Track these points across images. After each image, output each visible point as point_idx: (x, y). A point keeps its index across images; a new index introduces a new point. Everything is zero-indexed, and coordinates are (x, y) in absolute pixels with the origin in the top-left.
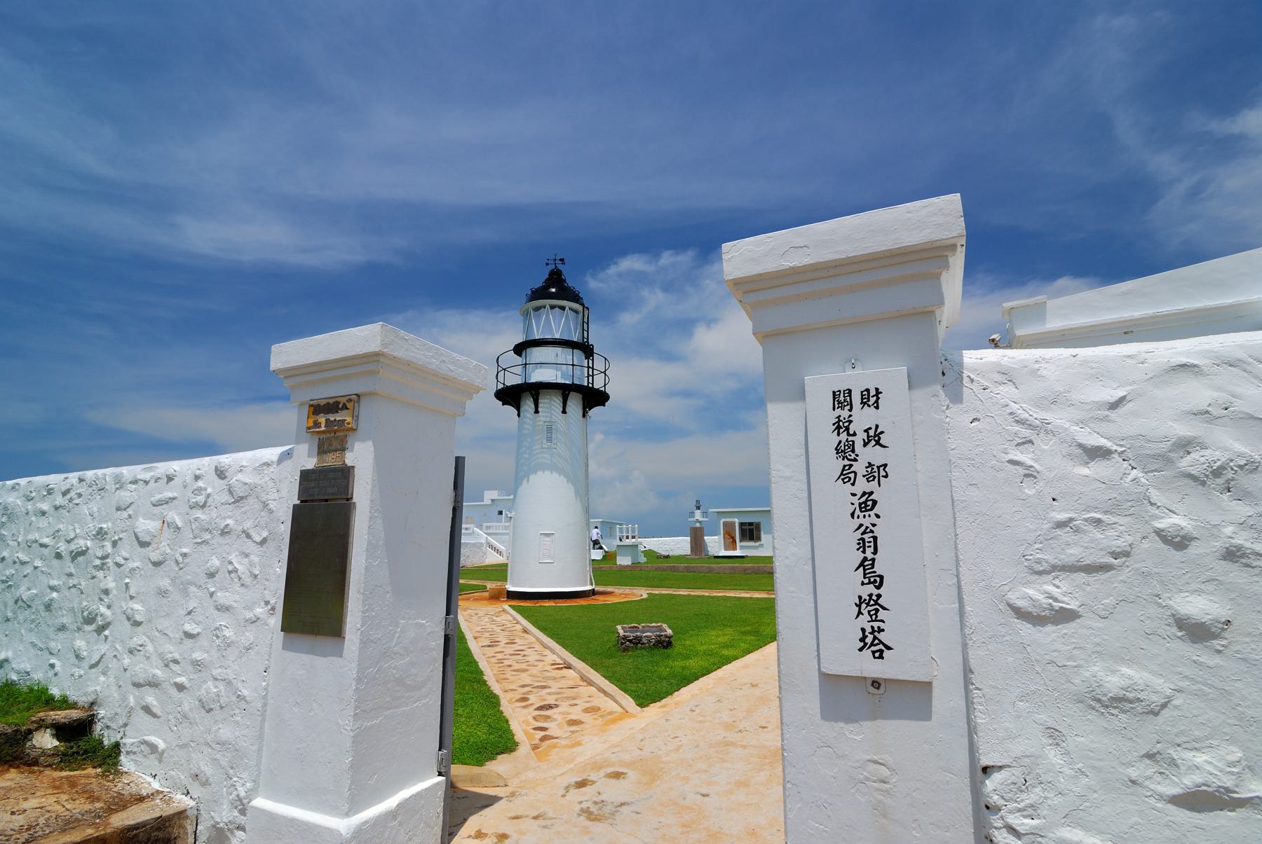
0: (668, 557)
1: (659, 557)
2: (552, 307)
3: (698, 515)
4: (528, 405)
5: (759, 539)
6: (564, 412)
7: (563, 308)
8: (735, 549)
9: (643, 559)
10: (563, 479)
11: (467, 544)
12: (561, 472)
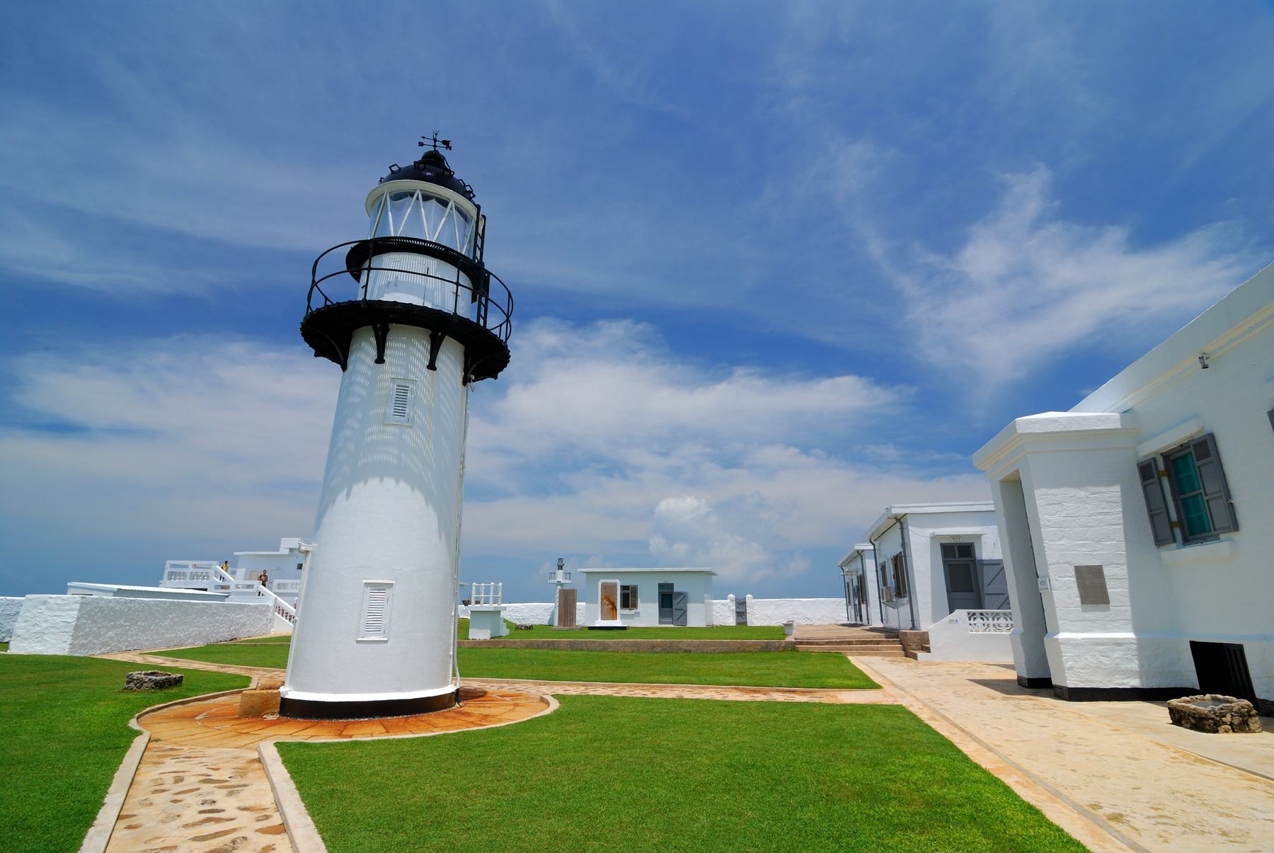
0: (530, 628)
1: (518, 628)
2: (426, 198)
3: (560, 576)
4: (363, 350)
5: (635, 606)
6: (432, 366)
7: (444, 203)
8: (614, 618)
9: (505, 632)
10: (418, 498)
11: (1067, 642)
12: (416, 482)
